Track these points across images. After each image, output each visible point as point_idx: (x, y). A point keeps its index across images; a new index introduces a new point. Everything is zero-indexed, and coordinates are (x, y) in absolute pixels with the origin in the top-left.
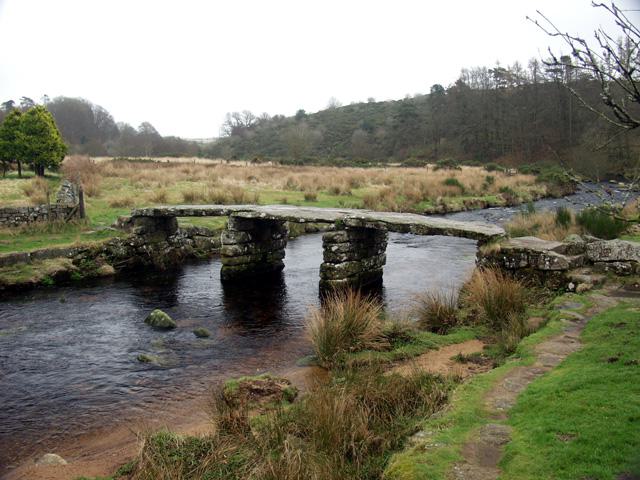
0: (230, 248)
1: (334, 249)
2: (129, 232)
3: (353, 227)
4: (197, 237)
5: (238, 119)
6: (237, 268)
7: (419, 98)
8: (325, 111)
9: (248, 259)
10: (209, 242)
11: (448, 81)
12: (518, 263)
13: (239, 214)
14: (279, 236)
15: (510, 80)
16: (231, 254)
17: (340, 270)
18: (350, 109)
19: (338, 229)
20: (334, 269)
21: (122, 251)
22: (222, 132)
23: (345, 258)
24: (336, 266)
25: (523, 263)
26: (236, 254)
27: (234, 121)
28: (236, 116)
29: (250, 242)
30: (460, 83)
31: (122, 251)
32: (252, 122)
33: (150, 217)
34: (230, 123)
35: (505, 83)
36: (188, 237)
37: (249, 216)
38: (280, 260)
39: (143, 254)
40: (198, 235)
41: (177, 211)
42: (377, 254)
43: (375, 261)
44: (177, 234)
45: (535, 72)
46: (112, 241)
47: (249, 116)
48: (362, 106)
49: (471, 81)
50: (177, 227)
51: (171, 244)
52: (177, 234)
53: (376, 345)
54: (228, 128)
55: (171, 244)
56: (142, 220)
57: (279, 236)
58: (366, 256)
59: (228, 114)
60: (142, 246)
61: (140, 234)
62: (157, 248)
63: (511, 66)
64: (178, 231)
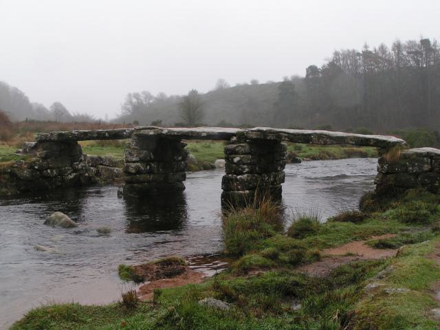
0: (133, 165)
1: (237, 159)
2: (35, 156)
3: (254, 139)
4: (101, 166)
5: (138, 99)
6: (140, 186)
7: (296, 79)
8: (214, 92)
9: (151, 177)
10: (112, 171)
11: (321, 61)
12: (420, 167)
13: (142, 132)
14: (180, 158)
15: (377, 63)
16: (133, 171)
17: (242, 181)
18: (238, 89)
19: (238, 141)
20: (237, 180)
21: (26, 173)
22: (124, 111)
23: (247, 170)
24: (238, 177)
25: (426, 167)
26: (139, 172)
27: (134, 100)
28: (136, 96)
29: (153, 161)
30: (332, 64)
31: (26, 173)
32: (151, 101)
33: (54, 141)
34: (131, 102)
35: (372, 65)
36: (92, 166)
37: (152, 133)
38: (181, 182)
39: (48, 178)
40: (102, 164)
41: (81, 134)
42: (277, 171)
43: (275, 177)
44: (81, 161)
45: (398, 54)
46: (16, 163)
47: (148, 96)
48: (246, 86)
49: (341, 62)
50: (81, 153)
51: (75, 170)
52: (81, 161)
53: (351, 142)
54: (129, 107)
55: (75, 170)
56: (46, 145)
57: (180, 158)
58: (267, 172)
59: (130, 95)
60: (46, 169)
61: (45, 158)
62: (61, 173)
63: (377, 48)
64: (82, 158)
